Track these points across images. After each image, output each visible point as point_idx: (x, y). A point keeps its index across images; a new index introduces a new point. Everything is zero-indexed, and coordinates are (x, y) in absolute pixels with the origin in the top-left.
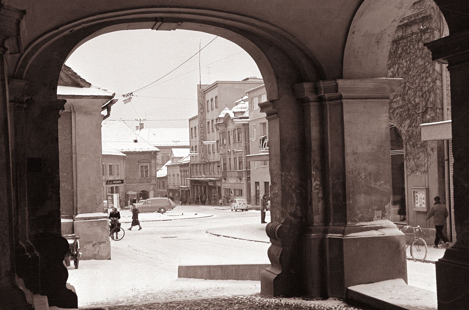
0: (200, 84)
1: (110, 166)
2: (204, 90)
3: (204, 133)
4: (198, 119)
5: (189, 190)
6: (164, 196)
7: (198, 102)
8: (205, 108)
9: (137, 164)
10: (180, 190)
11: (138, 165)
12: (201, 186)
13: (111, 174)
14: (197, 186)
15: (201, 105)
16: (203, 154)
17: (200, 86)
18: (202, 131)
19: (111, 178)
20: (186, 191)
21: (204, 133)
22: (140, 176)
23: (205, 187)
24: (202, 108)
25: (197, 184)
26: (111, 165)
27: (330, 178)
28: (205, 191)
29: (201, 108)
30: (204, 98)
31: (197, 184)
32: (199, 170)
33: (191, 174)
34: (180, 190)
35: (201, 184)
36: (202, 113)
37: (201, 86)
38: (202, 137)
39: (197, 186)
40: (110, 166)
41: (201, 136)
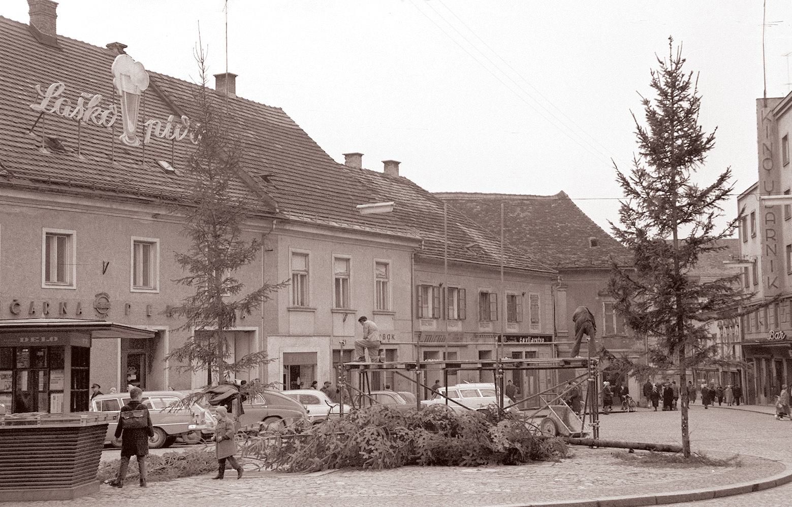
0: (763, 97)
1: (512, 298)
2: (775, 112)
3: (774, 221)
4: (758, 191)
5: (739, 371)
6: (115, 356)
7: (759, 142)
8: (778, 155)
9: (597, 298)
10: (721, 371)
11: (599, 302)
12: (768, 361)
13: (513, 317)
14: (759, 360)
15: (768, 149)
16: (772, 277)
17: (764, 102)
18: (771, 234)
19: (514, 330)
20: (733, 373)
21: (774, 221)
22: (605, 329)
23: (779, 364)
24: (769, 157)
25: (758, 356)
26: (513, 296)
27: (212, 450)
28: (779, 373)
29: (767, 159)
30: (775, 131)
31: (758, 356)
32: (762, 320)
33: (743, 331)
34: (721, 371)
35: (769, 356)
36: (769, 170)
37: (769, 102)
38: (769, 231)
39: (759, 360)
40: (512, 298)
41: (767, 230)
